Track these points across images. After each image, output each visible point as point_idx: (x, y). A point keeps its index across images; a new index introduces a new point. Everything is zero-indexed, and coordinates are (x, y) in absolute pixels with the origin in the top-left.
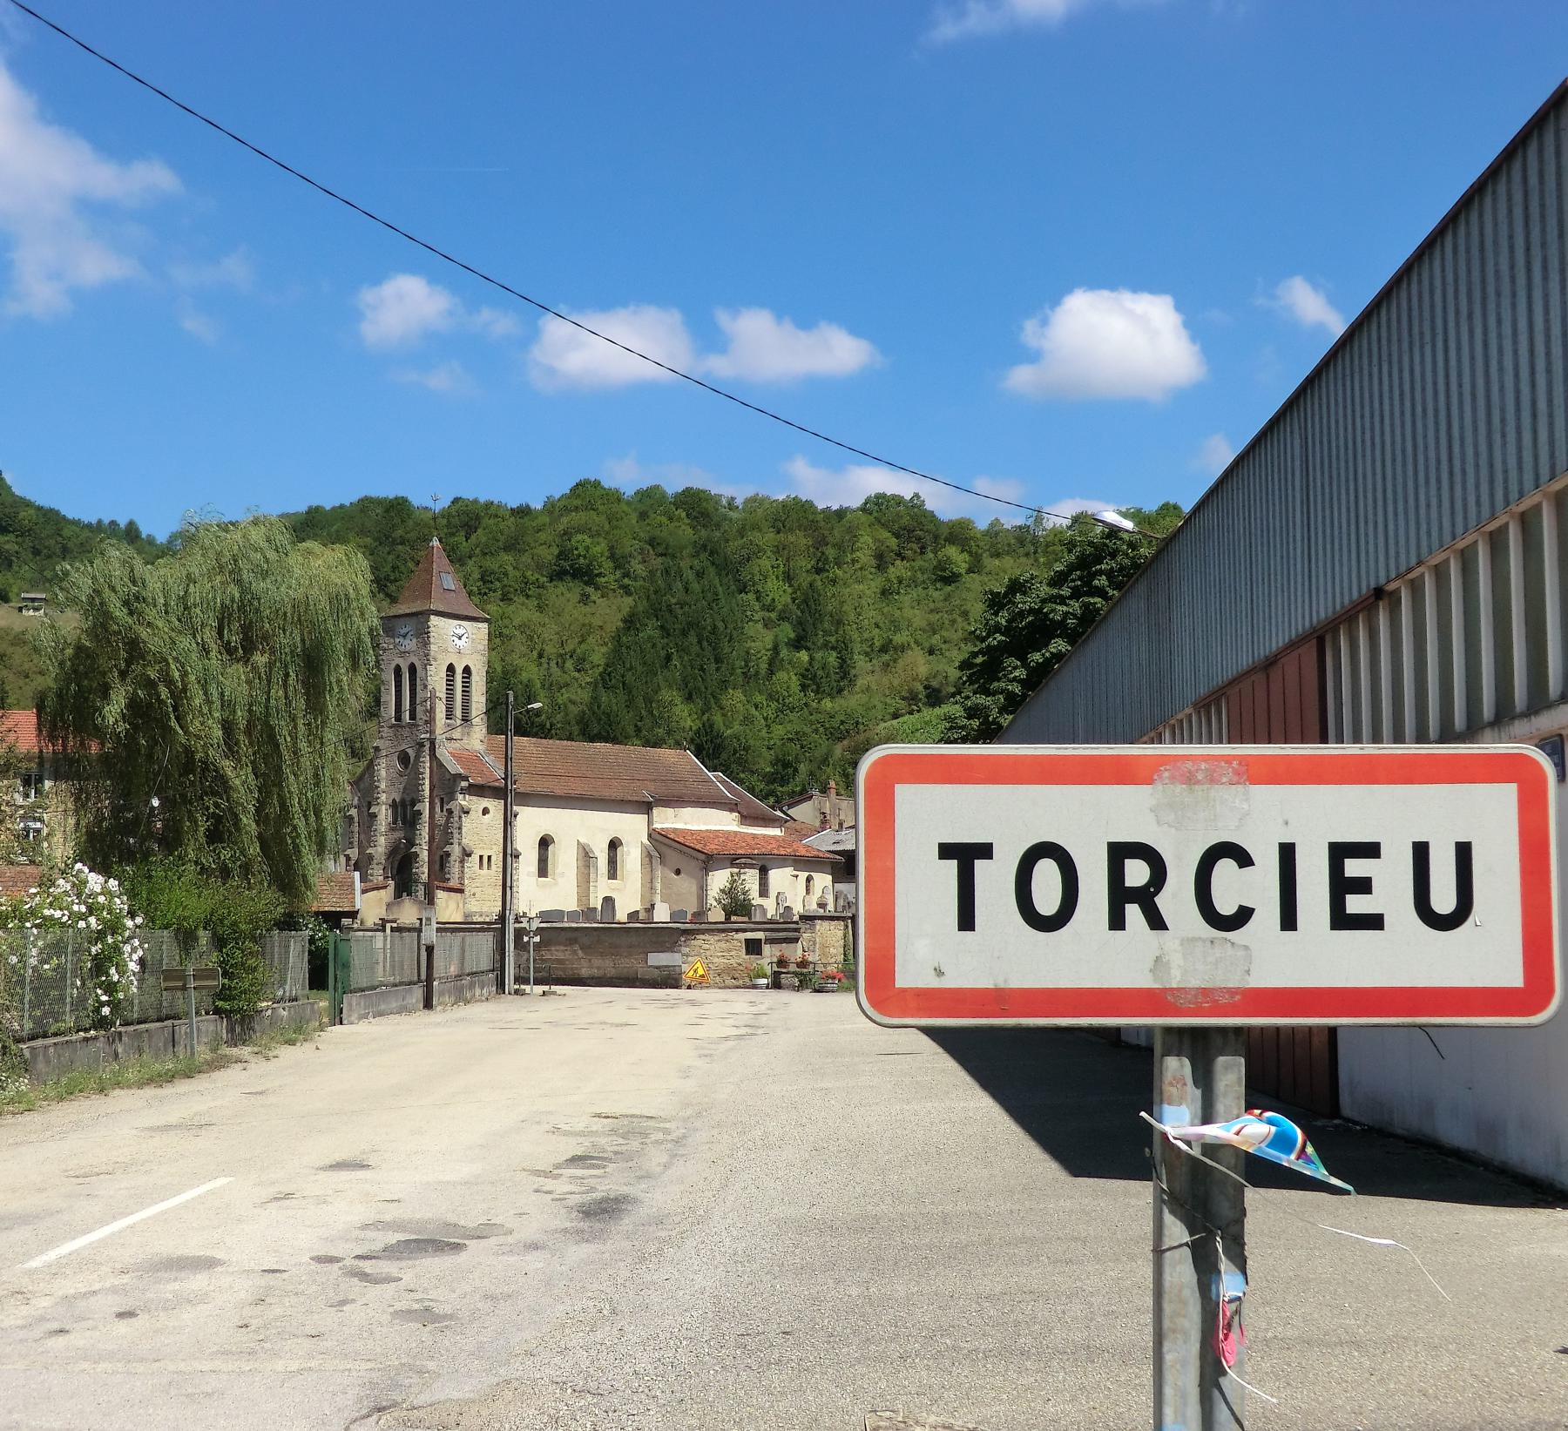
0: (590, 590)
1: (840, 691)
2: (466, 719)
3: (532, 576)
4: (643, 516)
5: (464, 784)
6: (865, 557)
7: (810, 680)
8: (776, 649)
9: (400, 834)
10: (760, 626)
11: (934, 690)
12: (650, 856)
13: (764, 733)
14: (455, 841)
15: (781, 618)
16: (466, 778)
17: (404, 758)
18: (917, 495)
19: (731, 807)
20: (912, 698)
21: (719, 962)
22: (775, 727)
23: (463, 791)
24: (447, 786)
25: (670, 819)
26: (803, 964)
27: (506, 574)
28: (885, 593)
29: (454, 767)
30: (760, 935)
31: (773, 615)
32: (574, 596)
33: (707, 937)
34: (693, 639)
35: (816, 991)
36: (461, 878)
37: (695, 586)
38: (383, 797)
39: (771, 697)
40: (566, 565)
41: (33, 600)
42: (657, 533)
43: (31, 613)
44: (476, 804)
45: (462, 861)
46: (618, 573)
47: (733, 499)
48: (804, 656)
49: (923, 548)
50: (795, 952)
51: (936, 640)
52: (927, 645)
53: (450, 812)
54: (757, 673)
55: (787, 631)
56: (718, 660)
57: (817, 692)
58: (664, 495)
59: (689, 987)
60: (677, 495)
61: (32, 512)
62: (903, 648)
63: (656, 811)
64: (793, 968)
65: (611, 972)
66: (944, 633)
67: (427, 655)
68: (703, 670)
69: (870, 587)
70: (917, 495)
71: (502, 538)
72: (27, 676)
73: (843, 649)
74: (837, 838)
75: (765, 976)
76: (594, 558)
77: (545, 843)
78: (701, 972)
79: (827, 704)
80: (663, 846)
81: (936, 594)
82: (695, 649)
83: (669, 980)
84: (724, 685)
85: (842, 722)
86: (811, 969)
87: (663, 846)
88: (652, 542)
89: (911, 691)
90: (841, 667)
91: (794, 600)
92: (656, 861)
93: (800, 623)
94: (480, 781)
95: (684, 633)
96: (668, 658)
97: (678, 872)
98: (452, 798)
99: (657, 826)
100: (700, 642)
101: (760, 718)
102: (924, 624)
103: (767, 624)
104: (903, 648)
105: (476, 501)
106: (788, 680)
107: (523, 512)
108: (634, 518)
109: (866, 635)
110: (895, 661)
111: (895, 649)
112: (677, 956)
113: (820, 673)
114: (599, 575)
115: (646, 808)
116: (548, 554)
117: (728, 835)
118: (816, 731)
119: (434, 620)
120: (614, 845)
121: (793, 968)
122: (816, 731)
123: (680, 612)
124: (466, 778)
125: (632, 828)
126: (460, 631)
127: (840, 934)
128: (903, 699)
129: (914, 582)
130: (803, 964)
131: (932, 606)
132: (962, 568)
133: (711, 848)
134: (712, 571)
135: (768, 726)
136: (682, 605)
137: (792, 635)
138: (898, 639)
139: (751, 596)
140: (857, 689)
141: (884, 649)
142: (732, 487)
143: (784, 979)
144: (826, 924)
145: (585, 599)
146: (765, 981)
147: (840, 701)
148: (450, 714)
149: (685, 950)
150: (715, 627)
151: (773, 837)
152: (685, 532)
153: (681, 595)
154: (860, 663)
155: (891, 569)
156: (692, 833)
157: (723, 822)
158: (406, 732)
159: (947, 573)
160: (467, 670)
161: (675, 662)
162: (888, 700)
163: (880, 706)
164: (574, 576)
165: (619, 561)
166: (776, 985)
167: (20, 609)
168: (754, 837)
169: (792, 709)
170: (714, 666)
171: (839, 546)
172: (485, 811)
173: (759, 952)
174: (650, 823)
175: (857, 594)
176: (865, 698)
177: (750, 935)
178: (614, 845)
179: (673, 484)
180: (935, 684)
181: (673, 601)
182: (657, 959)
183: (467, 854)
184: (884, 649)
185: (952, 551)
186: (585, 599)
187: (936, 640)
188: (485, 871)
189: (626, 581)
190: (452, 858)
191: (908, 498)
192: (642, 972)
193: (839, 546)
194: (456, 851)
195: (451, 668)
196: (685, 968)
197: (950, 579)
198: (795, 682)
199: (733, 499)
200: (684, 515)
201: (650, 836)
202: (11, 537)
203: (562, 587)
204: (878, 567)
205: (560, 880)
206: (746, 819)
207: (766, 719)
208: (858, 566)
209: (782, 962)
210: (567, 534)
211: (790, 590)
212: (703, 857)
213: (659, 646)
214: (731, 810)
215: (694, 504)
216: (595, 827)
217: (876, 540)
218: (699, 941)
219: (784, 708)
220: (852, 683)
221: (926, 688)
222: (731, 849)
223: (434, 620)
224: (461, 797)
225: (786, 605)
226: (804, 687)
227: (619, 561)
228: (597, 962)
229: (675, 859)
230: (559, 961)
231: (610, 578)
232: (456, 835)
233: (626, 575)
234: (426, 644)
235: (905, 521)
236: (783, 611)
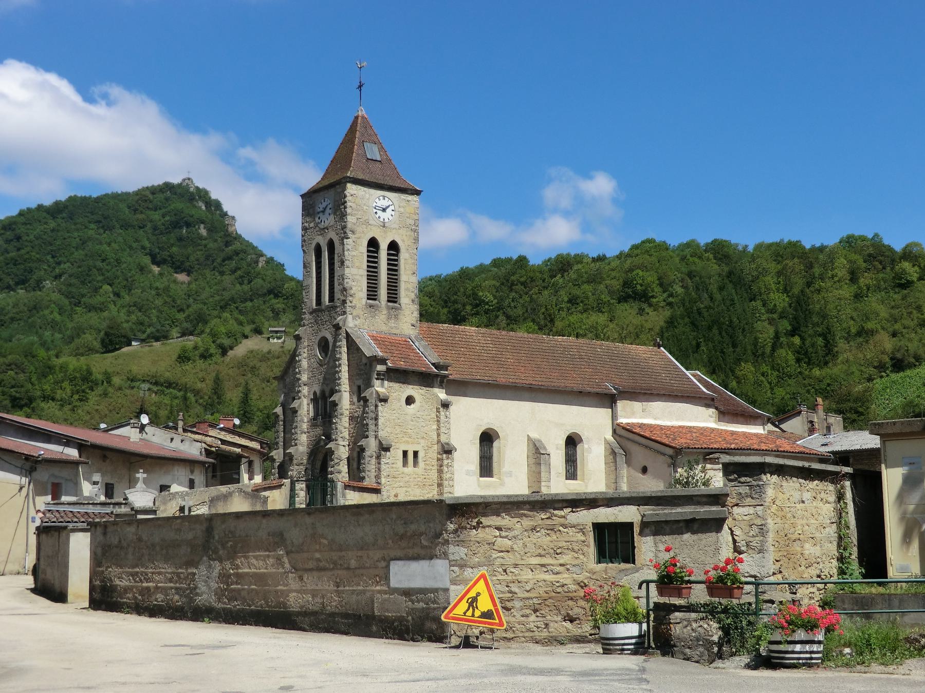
0: (645, 306)
1: (826, 363)
2: (393, 297)
3: (605, 297)
4: (683, 259)
5: (380, 368)
6: (842, 273)
7: (803, 356)
8: (777, 336)
9: (319, 431)
10: (766, 324)
11: (898, 360)
12: (614, 453)
13: (769, 394)
14: (371, 433)
15: (781, 317)
16: (383, 361)
17: (324, 345)
18: (876, 235)
19: (707, 402)
20: (881, 367)
21: (533, 579)
22: (776, 390)
23: (381, 376)
24: (364, 369)
25: (634, 414)
26: (724, 584)
27: (587, 298)
28: (858, 297)
29: (370, 349)
30: (629, 514)
31: (775, 316)
32: (634, 311)
33: (505, 520)
34: (715, 331)
35: (767, 662)
36: (378, 477)
37: (718, 296)
38: (305, 390)
39: (773, 368)
40: (630, 291)
41: (277, 332)
42: (693, 268)
43: (275, 340)
44: (397, 391)
45: (378, 457)
46: (665, 295)
47: (746, 246)
48: (797, 340)
49: (884, 268)
50: (700, 555)
51: (897, 326)
52: (891, 330)
53: (366, 400)
54: (763, 353)
55: (785, 325)
56: (734, 346)
57: (808, 364)
58: (698, 245)
59: (467, 643)
60: (707, 245)
61: (293, 283)
62: (872, 332)
63: (620, 404)
64: (699, 595)
65: (333, 603)
66: (903, 321)
67: (344, 227)
68: (722, 352)
69: (847, 291)
70: (876, 235)
71: (586, 276)
72: (268, 381)
73: (827, 335)
74: (825, 441)
75: (631, 616)
76: (649, 285)
77: (487, 438)
78: (484, 604)
79: (816, 372)
80: (627, 440)
81: (896, 296)
82: (717, 338)
83: (420, 624)
84: (738, 361)
85: (829, 385)
86: (747, 596)
87: (627, 440)
88: (690, 275)
89: (880, 362)
90: (826, 346)
91: (790, 306)
92: (621, 460)
93: (795, 318)
94: (402, 365)
95: (710, 328)
96: (698, 345)
97: (644, 470)
98: (369, 385)
99: (623, 420)
100: (720, 334)
101: (766, 383)
102: (887, 316)
103: (771, 322)
104: (872, 332)
105: (568, 255)
106: (786, 355)
107: (601, 259)
108: (677, 260)
109: (845, 325)
110: (867, 342)
111: (867, 333)
112: (440, 565)
113: (810, 350)
114: (653, 297)
115: (609, 400)
116: (616, 285)
117: (703, 431)
118: (808, 392)
119: (351, 189)
120: (572, 442)
121: (699, 595)
122: (808, 392)
123: (706, 314)
124: (383, 361)
125: (594, 424)
126: (384, 203)
127: (828, 510)
128: (875, 367)
129: (878, 288)
130: (724, 584)
131: (893, 303)
132: (915, 277)
133: (680, 442)
134: (730, 286)
135: (772, 389)
136: (708, 308)
137: (789, 328)
138: (870, 325)
139: (758, 303)
140: (839, 361)
141: (859, 334)
142: (747, 234)
143: (682, 626)
144: (792, 485)
145: (641, 311)
146: (631, 630)
147: (826, 371)
148: (372, 293)
149: (457, 552)
150: (731, 321)
151: (756, 435)
152: (714, 268)
153: (707, 302)
154: (842, 345)
155: (862, 280)
156: (661, 428)
157: (698, 419)
158: (325, 317)
159: (903, 281)
160: (393, 247)
161: (703, 348)
162: (863, 368)
163: (857, 373)
164: (635, 299)
165: (664, 285)
166: (658, 641)
167: (268, 339)
168: (733, 433)
169: (790, 377)
170: (731, 349)
171: (824, 266)
172: (410, 400)
173: (629, 556)
174: (614, 417)
175: (836, 296)
176: (845, 367)
177: (605, 515)
178: (572, 442)
179: (704, 239)
180: (899, 356)
181: (702, 306)
182: (407, 574)
183: (384, 448)
184: (859, 334)
185: (906, 265)
186: (641, 311)
187: (897, 326)
188: (410, 468)
189: (671, 299)
190: (367, 453)
191: (870, 236)
192: (386, 607)
193: (824, 266)
194: (371, 445)
195: (373, 244)
196: (455, 591)
197: (907, 285)
198: (791, 357)
199: (746, 246)
200: (711, 256)
201: (614, 431)
202: (281, 300)
203: (626, 306)
204: (851, 280)
205: (506, 480)
206: (727, 413)
207: (770, 383)
208: (836, 279)
209: (670, 580)
210: (631, 270)
211: (787, 299)
212: (670, 451)
213: (691, 337)
214: (708, 406)
215: (720, 251)
216: (551, 421)
217: (850, 261)
218: (488, 530)
219: (783, 376)
220: (835, 356)
221: (892, 359)
222: (704, 443)
223: (351, 189)
224: (377, 383)
225: (784, 308)
226: (798, 360)
227: (664, 285)
228: (311, 582)
229: (641, 456)
230: (260, 578)
231: (660, 297)
232: (372, 427)
233: (671, 295)
234: (343, 216)
235: (871, 251)
236: (782, 312)
